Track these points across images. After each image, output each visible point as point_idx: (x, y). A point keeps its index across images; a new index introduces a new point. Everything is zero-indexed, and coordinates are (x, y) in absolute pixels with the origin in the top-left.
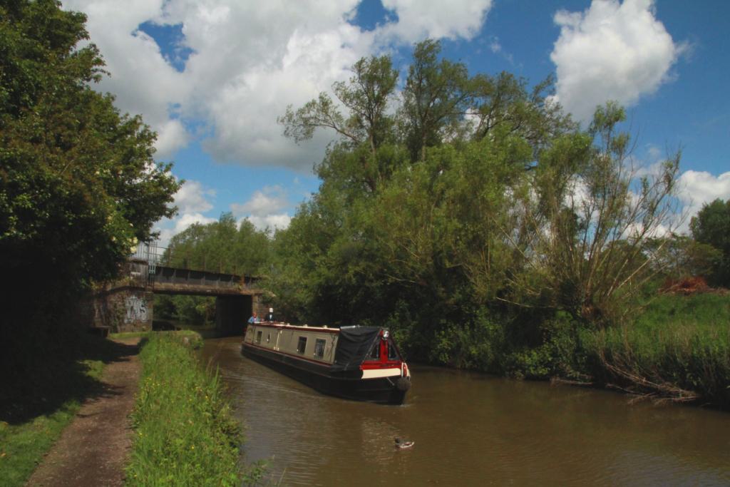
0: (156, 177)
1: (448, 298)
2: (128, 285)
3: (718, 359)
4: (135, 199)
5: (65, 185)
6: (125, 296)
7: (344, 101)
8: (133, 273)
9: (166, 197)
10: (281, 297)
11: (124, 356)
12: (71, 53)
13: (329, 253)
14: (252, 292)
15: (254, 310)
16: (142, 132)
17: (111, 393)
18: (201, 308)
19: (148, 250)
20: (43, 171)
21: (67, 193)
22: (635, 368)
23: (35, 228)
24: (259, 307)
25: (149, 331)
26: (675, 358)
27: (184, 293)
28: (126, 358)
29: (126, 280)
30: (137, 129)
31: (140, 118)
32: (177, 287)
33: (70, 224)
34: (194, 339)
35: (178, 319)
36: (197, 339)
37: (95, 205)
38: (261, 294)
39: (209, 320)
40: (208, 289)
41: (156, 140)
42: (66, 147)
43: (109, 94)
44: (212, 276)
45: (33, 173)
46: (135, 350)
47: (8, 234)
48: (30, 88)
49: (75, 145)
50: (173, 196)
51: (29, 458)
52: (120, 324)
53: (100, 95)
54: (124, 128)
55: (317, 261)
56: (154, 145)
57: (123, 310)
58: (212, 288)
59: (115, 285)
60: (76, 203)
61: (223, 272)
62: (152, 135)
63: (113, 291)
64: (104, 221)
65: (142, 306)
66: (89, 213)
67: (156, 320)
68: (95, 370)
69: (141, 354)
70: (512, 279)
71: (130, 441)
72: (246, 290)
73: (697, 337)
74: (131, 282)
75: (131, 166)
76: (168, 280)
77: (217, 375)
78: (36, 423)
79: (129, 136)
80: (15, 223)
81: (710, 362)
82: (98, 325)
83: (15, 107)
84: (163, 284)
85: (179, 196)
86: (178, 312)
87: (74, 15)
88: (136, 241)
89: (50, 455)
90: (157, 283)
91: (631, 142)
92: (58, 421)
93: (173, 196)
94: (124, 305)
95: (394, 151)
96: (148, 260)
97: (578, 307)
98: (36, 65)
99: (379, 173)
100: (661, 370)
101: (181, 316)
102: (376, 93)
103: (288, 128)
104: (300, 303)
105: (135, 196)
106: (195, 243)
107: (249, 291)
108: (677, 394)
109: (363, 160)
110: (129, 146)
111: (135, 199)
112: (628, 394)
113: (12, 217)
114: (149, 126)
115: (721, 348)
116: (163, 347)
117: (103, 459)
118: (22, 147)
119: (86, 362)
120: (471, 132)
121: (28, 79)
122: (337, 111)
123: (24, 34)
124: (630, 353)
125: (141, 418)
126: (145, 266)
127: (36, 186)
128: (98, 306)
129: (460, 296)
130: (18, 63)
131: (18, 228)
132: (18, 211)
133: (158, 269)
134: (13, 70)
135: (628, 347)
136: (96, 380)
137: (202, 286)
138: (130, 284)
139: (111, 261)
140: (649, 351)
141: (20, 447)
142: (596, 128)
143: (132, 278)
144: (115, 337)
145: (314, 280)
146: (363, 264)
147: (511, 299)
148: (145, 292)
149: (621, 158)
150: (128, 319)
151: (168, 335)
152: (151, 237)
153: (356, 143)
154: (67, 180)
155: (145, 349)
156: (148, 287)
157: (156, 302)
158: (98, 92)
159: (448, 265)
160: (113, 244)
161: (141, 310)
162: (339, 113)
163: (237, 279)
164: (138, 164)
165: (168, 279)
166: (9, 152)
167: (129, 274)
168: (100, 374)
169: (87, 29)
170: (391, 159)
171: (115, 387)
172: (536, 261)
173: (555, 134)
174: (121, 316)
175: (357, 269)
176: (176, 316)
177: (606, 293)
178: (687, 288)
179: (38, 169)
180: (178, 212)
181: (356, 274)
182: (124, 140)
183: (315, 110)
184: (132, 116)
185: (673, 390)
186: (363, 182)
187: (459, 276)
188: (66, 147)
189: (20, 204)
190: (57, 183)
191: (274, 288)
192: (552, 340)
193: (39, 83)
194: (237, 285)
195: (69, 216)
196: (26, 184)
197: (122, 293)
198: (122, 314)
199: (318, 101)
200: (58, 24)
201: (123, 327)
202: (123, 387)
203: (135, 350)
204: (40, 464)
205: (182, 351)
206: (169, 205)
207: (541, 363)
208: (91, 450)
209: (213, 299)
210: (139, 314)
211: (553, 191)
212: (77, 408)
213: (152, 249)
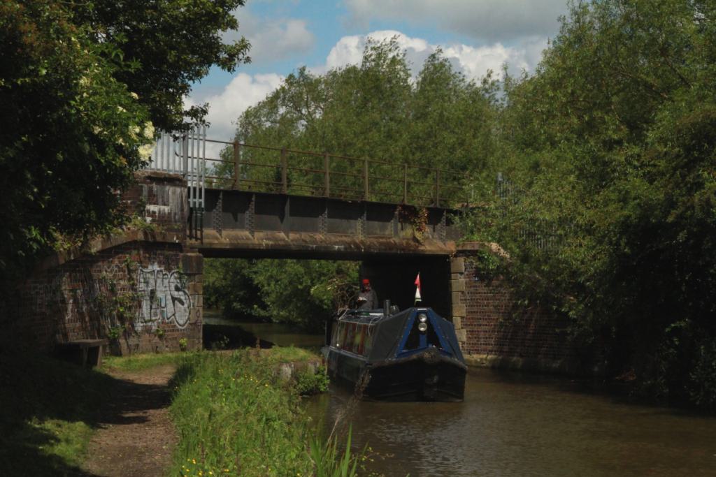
2: (140, 236)
4: (143, 26)
6: (135, 265)
8: (152, 208)
10: (525, 258)
11: (133, 411)
13: (650, 134)
15: (454, 294)
19: (186, 150)
25: (196, 349)
27: (279, 253)
28: (141, 414)
29: (134, 227)
32: (259, 239)
34: (305, 368)
35: (269, 320)
36: (312, 368)
37: (48, 52)
44: (345, 209)
46: (160, 397)
52: (127, 334)
55: (619, 156)
57: (133, 299)
63: (106, 254)
64: (70, 88)
65: (177, 289)
66: (35, 73)
67: (213, 322)
68: (68, 441)
72: (433, 242)
74: (147, 231)
76: (236, 223)
77: (348, 454)
82: (75, 338)
86: (267, 300)
88: (149, 131)
90: (209, 232)
104: (574, 274)
106: (301, 126)
107: (440, 244)
111: (143, 26)
116: (227, 387)
119: (49, 425)
126: (178, 190)
128: (73, 290)
133: (211, 195)
136: (72, 464)
137: (321, 234)
138: (145, 234)
139: (95, 184)
143: (149, 219)
144: (113, 366)
145: (608, 212)
151: (238, 359)
152: (187, 119)
155: (185, 391)
157: (214, 275)
160: (94, 139)
161: (174, 299)
163: (409, 214)
165: (236, 219)
167: (142, 212)
168: (83, 452)
173: (193, 28)
174: (127, 315)
176: (263, 313)
180: (248, 54)
194: (409, 232)
201: (133, 341)
203: (160, 397)
205: (270, 397)
206: (227, 37)
209: (353, 268)
210: (170, 309)
213: (194, 150)
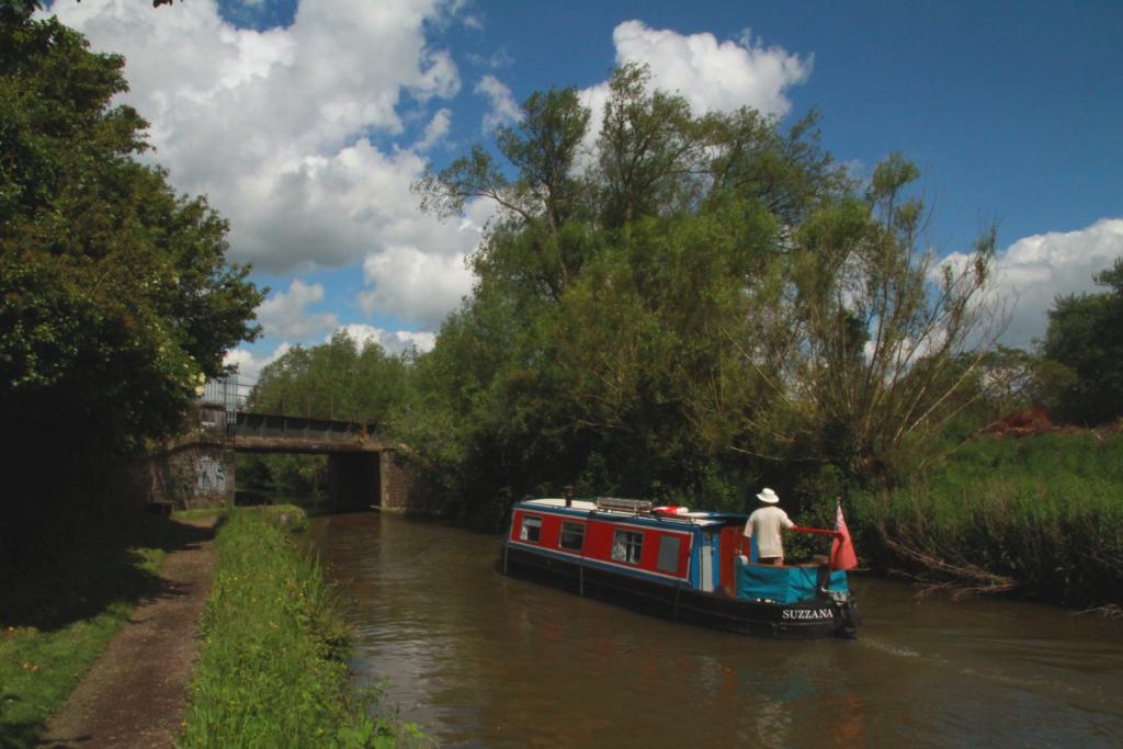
0: (228, 285)
1: (663, 449)
2: (197, 440)
3: (1046, 530)
4: (200, 317)
5: (98, 309)
7: (510, 157)
8: (205, 423)
9: (245, 313)
12: (104, 113)
14: (380, 447)
16: (208, 220)
17: (174, 592)
18: (308, 472)
20: (67, 292)
21: (101, 318)
22: (930, 545)
23: (60, 369)
24: (390, 468)
26: (985, 529)
29: (193, 434)
30: (201, 215)
31: (204, 199)
32: (269, 442)
33: (107, 360)
35: (274, 489)
36: (299, 516)
37: (140, 332)
38: (392, 450)
39: (319, 489)
40: (315, 443)
41: (228, 230)
42: (98, 254)
43: (159, 167)
45: (54, 294)
46: (208, 534)
47: (27, 379)
48: (49, 176)
49: (110, 251)
50: (256, 310)
51: (67, 672)
52: (189, 498)
53: (147, 169)
54: (182, 216)
56: (224, 238)
58: (320, 442)
59: (178, 440)
60: (114, 331)
61: (335, 419)
62: (223, 224)
63: (177, 450)
64: (153, 353)
65: (219, 471)
68: (152, 561)
69: (217, 538)
70: (752, 420)
71: (198, 653)
72: (370, 444)
73: (1017, 499)
74: (202, 437)
75: (194, 271)
76: (255, 432)
78: (73, 631)
79: (189, 227)
80: (34, 363)
81: (1033, 534)
82: (159, 499)
83: (31, 203)
84: (249, 438)
85: (264, 310)
86: (274, 477)
87: (107, 58)
88: (202, 378)
89: (93, 670)
91: (925, 212)
92: (103, 628)
93: (256, 310)
94: (193, 470)
95: (583, 232)
96: (225, 404)
97: (850, 459)
98: (56, 141)
99: (563, 265)
100: (966, 548)
101: (279, 484)
102: (557, 144)
103: (425, 199)
105: (200, 314)
108: (987, 582)
109: (536, 247)
110: (190, 242)
111: (200, 317)
112: (915, 584)
113: (29, 356)
114: (217, 212)
115: (1049, 513)
117: (162, 675)
118: (40, 260)
119: (141, 551)
120: (698, 196)
121: (44, 164)
122: (498, 172)
123: (39, 94)
124: (924, 525)
125: (211, 621)
127: (61, 313)
128: (157, 472)
129: (681, 445)
130: (31, 145)
131: (37, 369)
132: (39, 347)
133: (241, 416)
134: (26, 155)
135: (921, 517)
139: (168, 408)
140: (949, 520)
141: (55, 659)
142: (876, 193)
144: (181, 516)
146: (538, 402)
147: (752, 448)
148: (222, 451)
149: (910, 236)
150: (200, 490)
153: (528, 220)
154: (100, 303)
155: (223, 531)
156: (226, 443)
158: (144, 165)
159: (660, 399)
161: (218, 477)
162: (501, 175)
163: (356, 428)
164: (202, 267)
166: (23, 269)
167: (198, 424)
169: (125, 77)
170: (578, 245)
171: (179, 585)
172: (794, 391)
174: (190, 486)
175: (530, 410)
177: (892, 438)
178: (1020, 426)
179: (61, 289)
181: (528, 418)
182: (182, 233)
183: (467, 172)
184: (193, 198)
185: (981, 575)
186: (539, 278)
187: (675, 415)
188: (98, 254)
189: (40, 337)
190: (87, 306)
191: (409, 440)
192: (813, 508)
193: (60, 168)
194: (356, 438)
195: (105, 350)
196: (47, 310)
197: (190, 452)
198: (190, 482)
199: (470, 159)
200: (84, 75)
201: (193, 502)
202: (190, 584)
203: (208, 534)
204: (83, 680)
205: (272, 534)
206: (250, 324)
207: (797, 542)
208: (146, 664)
209: (324, 458)
210: (214, 482)
211: (819, 286)
212: (129, 611)
213: (230, 389)
